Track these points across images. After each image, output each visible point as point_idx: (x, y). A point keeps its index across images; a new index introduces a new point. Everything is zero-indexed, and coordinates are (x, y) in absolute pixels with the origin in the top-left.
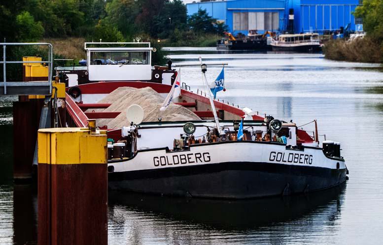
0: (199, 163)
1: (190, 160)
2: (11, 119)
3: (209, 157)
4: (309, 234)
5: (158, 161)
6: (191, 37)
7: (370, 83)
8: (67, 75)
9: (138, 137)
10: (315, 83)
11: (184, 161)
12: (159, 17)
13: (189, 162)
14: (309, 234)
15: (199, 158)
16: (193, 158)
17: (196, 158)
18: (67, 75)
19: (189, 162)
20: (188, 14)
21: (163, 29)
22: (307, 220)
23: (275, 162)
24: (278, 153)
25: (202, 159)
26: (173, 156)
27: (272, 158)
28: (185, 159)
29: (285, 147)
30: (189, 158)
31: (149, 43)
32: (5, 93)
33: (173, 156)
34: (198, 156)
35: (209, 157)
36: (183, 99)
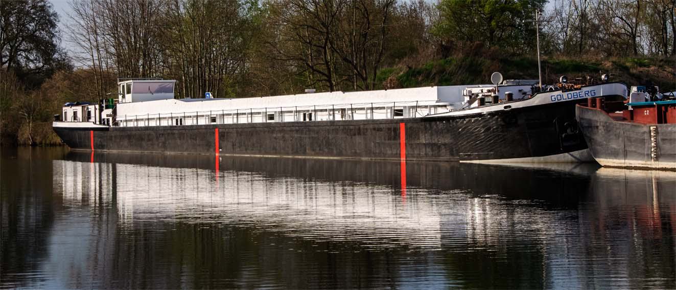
1: (581, 96)
3: (595, 93)
10: (638, 39)
17: (585, 94)
27: (553, 99)
28: (577, 95)
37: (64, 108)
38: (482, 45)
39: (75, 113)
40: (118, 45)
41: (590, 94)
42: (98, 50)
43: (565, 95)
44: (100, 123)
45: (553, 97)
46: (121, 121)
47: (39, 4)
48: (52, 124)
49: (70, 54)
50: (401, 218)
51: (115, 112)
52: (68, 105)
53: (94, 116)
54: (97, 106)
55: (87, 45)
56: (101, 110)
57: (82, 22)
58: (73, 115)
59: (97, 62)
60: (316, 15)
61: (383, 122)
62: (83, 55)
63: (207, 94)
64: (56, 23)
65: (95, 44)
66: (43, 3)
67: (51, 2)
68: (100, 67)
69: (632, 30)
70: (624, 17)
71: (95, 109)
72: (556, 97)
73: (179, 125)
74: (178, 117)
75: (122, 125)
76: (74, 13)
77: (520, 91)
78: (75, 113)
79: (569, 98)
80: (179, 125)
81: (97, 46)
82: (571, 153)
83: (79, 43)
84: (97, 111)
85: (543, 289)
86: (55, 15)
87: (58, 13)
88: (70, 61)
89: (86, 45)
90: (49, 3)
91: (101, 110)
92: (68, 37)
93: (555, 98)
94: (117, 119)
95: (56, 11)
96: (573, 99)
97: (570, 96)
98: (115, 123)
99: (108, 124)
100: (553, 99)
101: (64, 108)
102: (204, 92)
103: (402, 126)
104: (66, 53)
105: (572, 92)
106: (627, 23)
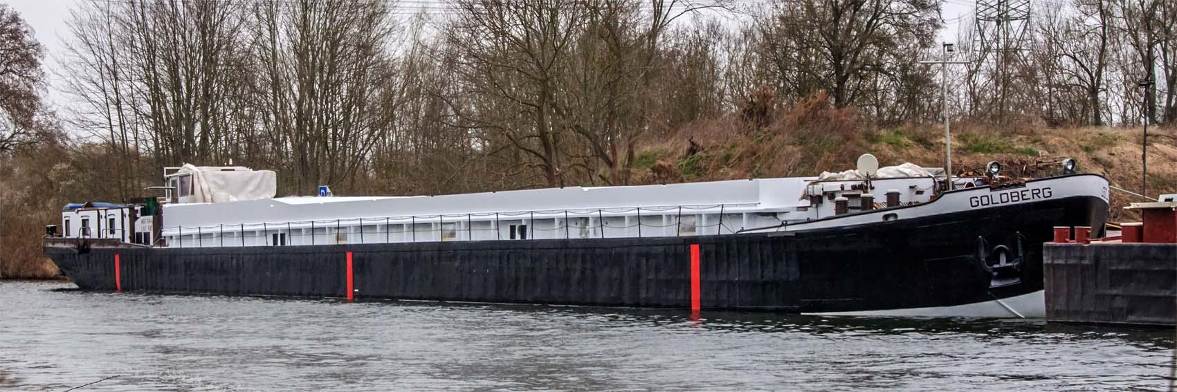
1: (1024, 197)
2: (1018, 280)
5: (978, 202)
7: (195, 340)
9: (960, 148)
12: (132, 183)
13: (1023, 199)
15: (1037, 194)
16: (1029, 195)
17: (1033, 194)
19: (1023, 199)
22: (584, 262)
23: (980, 207)
25: (1041, 195)
26: (1001, 195)
28: (1018, 196)
30: (1022, 195)
31: (165, 168)
32: (117, 257)
33: (1001, 195)
34: (1035, 192)
35: (1050, 192)
36: (743, 144)
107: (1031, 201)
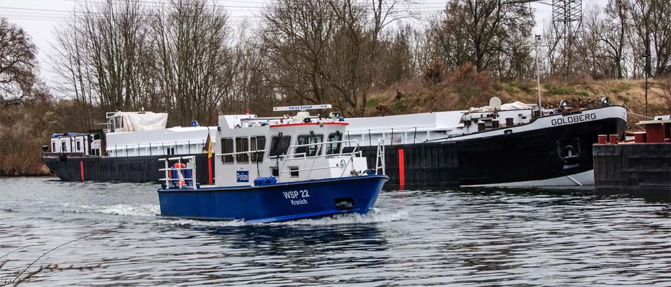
0: (588, 120)
1: (581, 119)
3: (595, 116)
4: (410, 241)
6: (334, 63)
8: (304, 123)
10: (622, 62)
11: (576, 120)
14: (410, 241)
15: (588, 117)
16: (583, 118)
17: (586, 117)
18: (304, 123)
20: (231, 42)
21: (586, 59)
24: (558, 120)
25: (590, 118)
27: (554, 123)
28: (578, 119)
29: (151, 191)
30: (580, 118)
34: (587, 116)
35: (595, 116)
37: (52, 140)
38: (470, 70)
39: (63, 144)
40: (101, 75)
41: (590, 118)
42: (81, 81)
43: (566, 118)
44: (90, 153)
45: (554, 121)
46: (111, 151)
47: (18, 37)
48: (635, 138)
49: (48, 84)
50: (430, 229)
51: (104, 144)
52: (56, 137)
53: (83, 146)
54: (86, 137)
55: (70, 75)
56: (90, 141)
57: (65, 53)
58: (61, 146)
59: (80, 92)
60: (304, 41)
61: (368, 149)
62: (67, 86)
63: (193, 122)
64: (35, 54)
65: (78, 74)
66: (21, 35)
67: (30, 34)
68: (84, 98)
69: (617, 53)
70: (609, 40)
71: (84, 140)
72: (557, 121)
73: (171, 154)
74: (169, 146)
75: (113, 155)
76: (57, 44)
77: (519, 115)
78: (63, 144)
79: (558, 124)
80: (171, 154)
81: (80, 77)
82: (568, 176)
83: (62, 74)
84: (87, 142)
85: (669, 172)
86: (33, 46)
87: (36, 45)
88: (48, 91)
89: (69, 76)
90: (28, 35)
91: (90, 141)
92: (51, 67)
93: (556, 122)
94: (107, 149)
95: (35, 43)
96: (573, 122)
97: (570, 120)
98: (105, 153)
99: (98, 154)
100: (554, 123)
101: (52, 140)
102: (190, 119)
103: (401, 152)
104: (44, 83)
105: (572, 116)
106: (611, 46)
107: (585, 121)
